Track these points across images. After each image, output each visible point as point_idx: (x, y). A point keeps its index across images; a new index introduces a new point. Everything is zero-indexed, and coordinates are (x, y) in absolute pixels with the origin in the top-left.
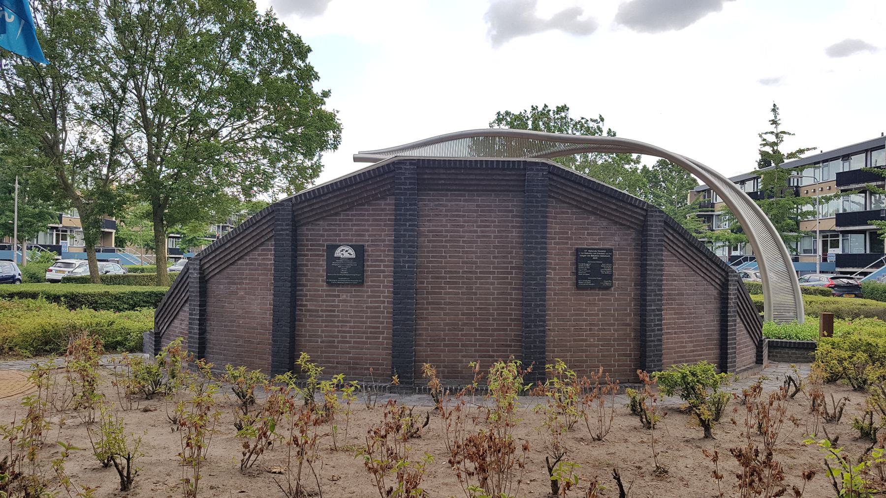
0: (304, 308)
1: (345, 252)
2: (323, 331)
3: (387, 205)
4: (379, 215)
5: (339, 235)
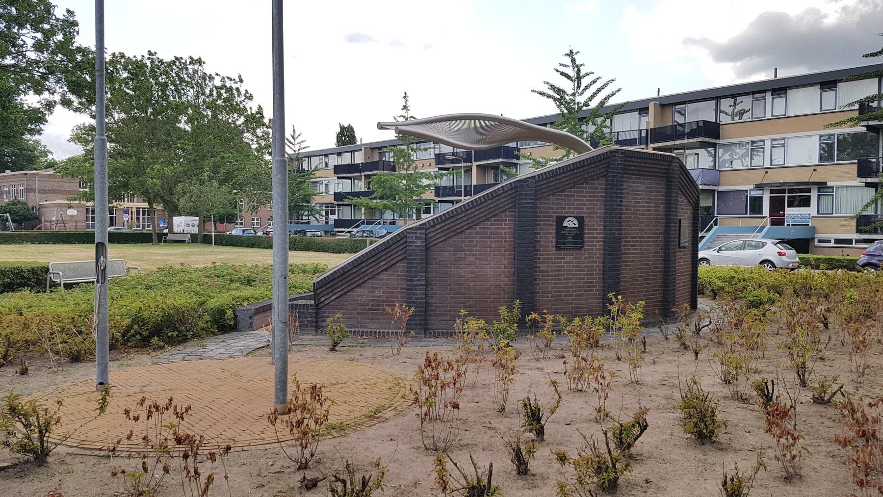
0: (537, 269)
1: (571, 223)
2: (552, 288)
3: (600, 184)
4: (594, 192)
5: (564, 208)
